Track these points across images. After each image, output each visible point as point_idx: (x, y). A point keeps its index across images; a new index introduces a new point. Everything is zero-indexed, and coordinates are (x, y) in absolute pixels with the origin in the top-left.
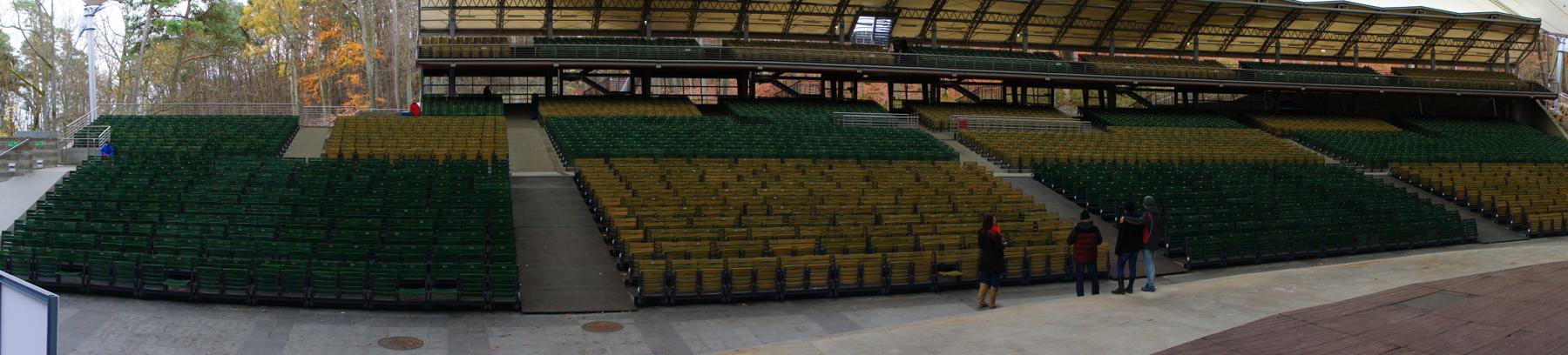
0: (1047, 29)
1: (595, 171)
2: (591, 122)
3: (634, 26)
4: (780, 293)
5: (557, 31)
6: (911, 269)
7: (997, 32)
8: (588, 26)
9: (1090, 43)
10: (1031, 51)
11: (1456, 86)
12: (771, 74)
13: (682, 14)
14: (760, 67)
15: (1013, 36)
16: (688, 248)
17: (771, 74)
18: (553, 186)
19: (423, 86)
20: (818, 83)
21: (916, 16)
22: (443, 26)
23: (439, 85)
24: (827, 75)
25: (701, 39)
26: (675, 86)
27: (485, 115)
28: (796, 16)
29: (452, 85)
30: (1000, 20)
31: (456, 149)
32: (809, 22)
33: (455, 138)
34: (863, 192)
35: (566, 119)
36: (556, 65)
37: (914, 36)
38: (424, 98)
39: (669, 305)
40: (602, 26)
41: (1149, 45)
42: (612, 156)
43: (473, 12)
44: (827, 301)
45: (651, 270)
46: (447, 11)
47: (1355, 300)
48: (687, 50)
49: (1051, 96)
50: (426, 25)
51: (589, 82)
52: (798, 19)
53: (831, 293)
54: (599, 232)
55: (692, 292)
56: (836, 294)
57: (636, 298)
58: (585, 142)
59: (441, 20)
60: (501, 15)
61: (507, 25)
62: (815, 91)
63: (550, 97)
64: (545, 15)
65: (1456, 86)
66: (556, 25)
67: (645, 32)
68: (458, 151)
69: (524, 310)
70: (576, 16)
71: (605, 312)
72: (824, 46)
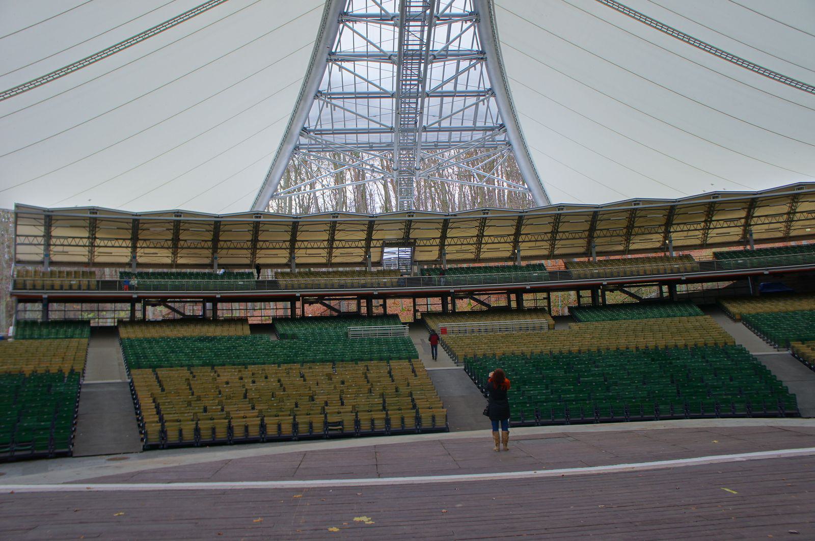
1: (144, 378)
2: (158, 342)
3: (508, 254)
7: (539, 248)
8: (169, 261)
9: (582, 250)
18: (113, 389)
19: (17, 312)
22: (39, 258)
23: (33, 312)
24: (360, 297)
26: (238, 310)
29: (46, 311)
32: (346, 253)
37: (435, 259)
38: (18, 323)
40: (180, 261)
41: (632, 247)
45: (153, 428)
47: (721, 428)
48: (534, 275)
49: (548, 298)
50: (21, 257)
54: (135, 415)
57: (144, 446)
58: (146, 357)
59: (37, 254)
61: (98, 259)
63: (133, 322)
64: (131, 252)
68: (43, 367)
70: (157, 254)
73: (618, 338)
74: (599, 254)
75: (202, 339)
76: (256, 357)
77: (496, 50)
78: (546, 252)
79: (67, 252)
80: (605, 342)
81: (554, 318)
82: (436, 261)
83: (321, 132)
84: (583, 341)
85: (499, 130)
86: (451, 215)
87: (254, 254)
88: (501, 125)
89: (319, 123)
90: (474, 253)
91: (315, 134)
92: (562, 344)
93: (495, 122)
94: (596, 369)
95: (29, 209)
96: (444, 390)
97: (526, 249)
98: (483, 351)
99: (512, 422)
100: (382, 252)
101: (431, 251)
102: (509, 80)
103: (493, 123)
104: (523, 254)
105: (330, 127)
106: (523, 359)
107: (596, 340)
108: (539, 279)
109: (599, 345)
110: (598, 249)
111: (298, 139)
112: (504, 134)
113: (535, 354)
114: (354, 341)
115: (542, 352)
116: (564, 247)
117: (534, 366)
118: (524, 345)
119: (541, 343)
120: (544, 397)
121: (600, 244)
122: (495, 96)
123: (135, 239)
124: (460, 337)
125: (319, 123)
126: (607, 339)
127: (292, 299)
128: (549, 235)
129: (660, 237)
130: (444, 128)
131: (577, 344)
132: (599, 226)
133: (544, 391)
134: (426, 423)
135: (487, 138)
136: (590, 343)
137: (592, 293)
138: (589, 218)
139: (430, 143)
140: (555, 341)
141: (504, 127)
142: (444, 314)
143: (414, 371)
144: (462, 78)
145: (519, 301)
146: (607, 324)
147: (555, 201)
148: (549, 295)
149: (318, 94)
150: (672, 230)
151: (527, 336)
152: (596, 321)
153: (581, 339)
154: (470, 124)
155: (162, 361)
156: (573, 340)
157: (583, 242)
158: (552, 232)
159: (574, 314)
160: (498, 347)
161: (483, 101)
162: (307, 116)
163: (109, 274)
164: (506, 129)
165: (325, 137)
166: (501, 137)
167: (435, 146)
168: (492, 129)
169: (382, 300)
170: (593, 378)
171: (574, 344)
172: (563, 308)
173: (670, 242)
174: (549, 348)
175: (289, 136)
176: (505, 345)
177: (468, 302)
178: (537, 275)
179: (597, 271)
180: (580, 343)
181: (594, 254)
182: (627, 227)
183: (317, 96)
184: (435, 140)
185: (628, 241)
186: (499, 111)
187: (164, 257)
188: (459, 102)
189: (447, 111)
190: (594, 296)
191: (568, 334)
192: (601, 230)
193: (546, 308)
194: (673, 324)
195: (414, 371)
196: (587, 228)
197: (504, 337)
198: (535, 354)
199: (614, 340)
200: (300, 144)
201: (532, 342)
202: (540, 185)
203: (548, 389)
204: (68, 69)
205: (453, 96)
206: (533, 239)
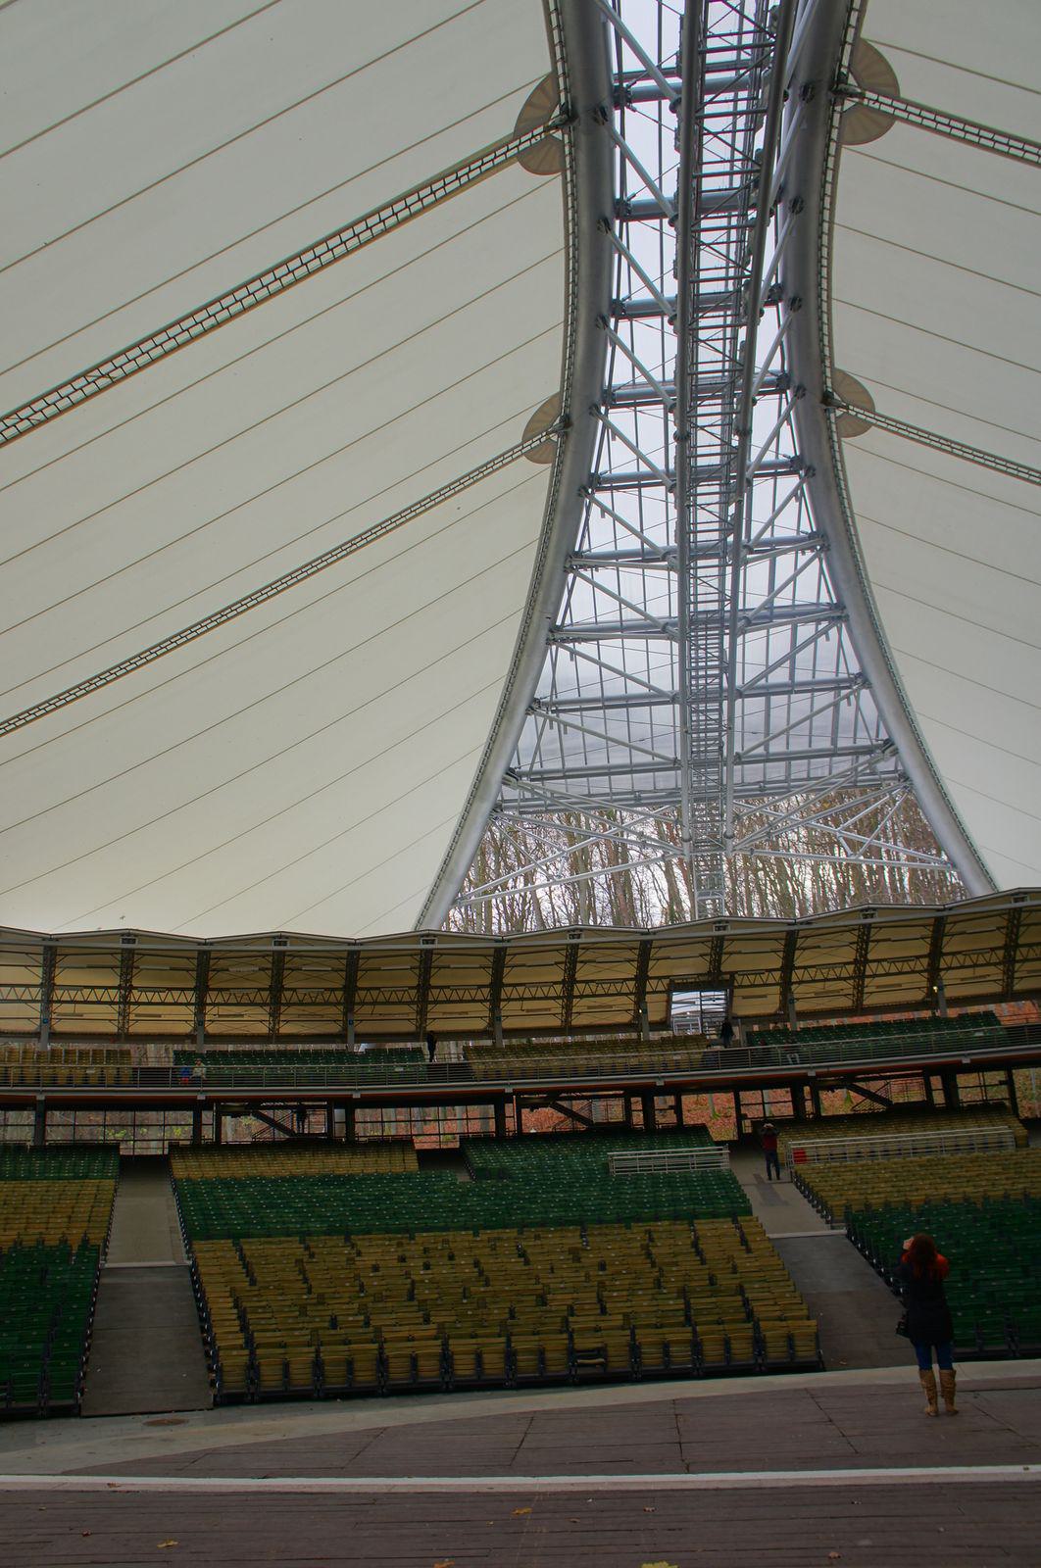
3: (920, 995)
4: (383, 1387)
8: (263, 1029)
11: (498, 1076)
13: (406, 1009)
16: (411, 1333)
18: (158, 1279)
27: (86, 1177)
31: (31, 1231)
33: (31, 1216)
35: (206, 1182)
39: (252, 1403)
40: (285, 1029)
42: (310, 1234)
43: (80, 1008)
44: (438, 1396)
46: (38, 1006)
48: (977, 1034)
49: (1009, 1083)
51: (561, 1109)
53: (758, 1369)
55: (307, 1385)
56: (256, 1398)
57: (215, 1396)
60: (124, 1015)
61: (137, 1028)
63: (197, 1147)
65: (498, 1076)
67: (937, 1002)
69: (84, 1413)
71: (176, 1411)
75: (326, 1180)
78: (996, 988)
82: (775, 1014)
83: (543, 776)
85: (883, 752)
91: (532, 780)
93: (873, 734)
98: (882, 1195)
100: (669, 1002)
101: (765, 996)
102: (896, 654)
104: (949, 993)
108: (985, 1043)
112: (894, 758)
115: (1006, 1196)
118: (968, 1181)
119: (1003, 1177)
123: (202, 989)
125: (537, 759)
130: (774, 754)
135: (860, 769)
140: (1034, 1172)
141: (892, 744)
143: (744, 1241)
144: (804, 657)
145: (950, 1089)
147: (1007, 882)
148: (1010, 1076)
151: (971, 1162)
154: (824, 743)
158: (1005, 947)
160: (914, 1187)
162: (515, 747)
163: (156, 1056)
166: (887, 765)
167: (761, 789)
176: (928, 1182)
177: (845, 1096)
178: (981, 1034)
183: (533, 709)
188: (801, 703)
189: (778, 720)
193: (1007, 1103)
206: (968, 962)
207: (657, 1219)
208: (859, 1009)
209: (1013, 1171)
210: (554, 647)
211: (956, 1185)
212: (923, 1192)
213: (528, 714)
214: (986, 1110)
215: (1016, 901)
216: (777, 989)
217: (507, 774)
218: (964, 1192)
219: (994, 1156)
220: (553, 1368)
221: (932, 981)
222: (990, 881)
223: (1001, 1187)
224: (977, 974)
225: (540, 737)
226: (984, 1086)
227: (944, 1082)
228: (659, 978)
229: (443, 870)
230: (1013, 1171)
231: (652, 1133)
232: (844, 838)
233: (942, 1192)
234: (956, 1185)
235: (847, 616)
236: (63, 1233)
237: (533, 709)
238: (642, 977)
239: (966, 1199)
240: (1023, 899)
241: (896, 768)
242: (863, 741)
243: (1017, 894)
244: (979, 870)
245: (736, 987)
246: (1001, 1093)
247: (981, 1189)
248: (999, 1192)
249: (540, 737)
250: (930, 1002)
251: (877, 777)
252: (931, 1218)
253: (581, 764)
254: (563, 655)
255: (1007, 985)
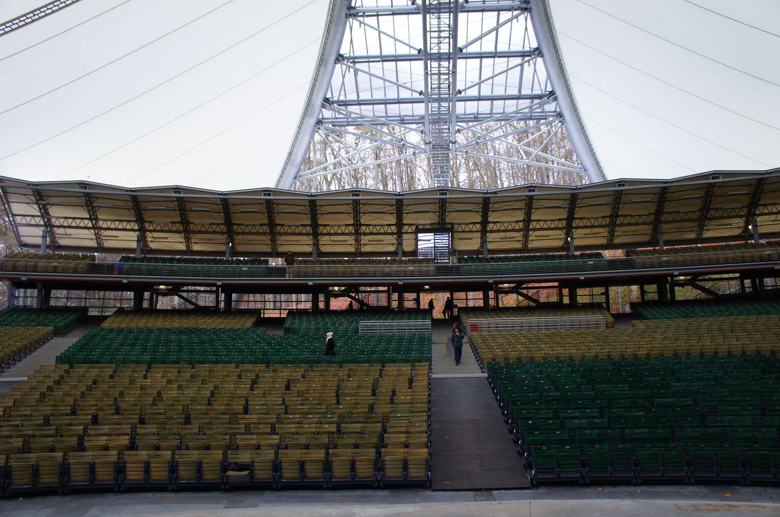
0: (595, 230)
3: (560, 243)
5: (490, 251)
6: (199, 466)
9: (646, 238)
10: (764, 241)
11: (306, 275)
12: (689, 277)
14: (676, 273)
15: (746, 228)
17: (689, 277)
20: (555, 291)
21: (549, 223)
25: (606, 251)
28: (616, 228)
30: (545, 226)
32: (376, 241)
34: (264, 393)
36: (491, 281)
40: (196, 247)
41: (706, 235)
43: (69, 231)
48: (590, 263)
49: (607, 294)
52: (365, 239)
62: (554, 299)
65: (306, 275)
66: (490, 246)
72: (737, 247)
73: (699, 339)
74: (667, 243)
75: (190, 331)
76: (512, 349)
77: (545, 9)
78: (604, 241)
79: (70, 235)
80: (683, 344)
81: (613, 315)
82: (478, 250)
83: (346, 104)
84: (653, 342)
85: (548, 98)
86: (491, 193)
87: (274, 241)
88: (551, 92)
89: (343, 93)
90: (521, 242)
91: (339, 105)
92: (624, 346)
93: (543, 88)
94: (678, 384)
95: (17, 183)
96: (448, 409)
97: (581, 238)
98: (517, 353)
99: (541, 476)
100: (417, 240)
101: (471, 239)
102: (558, 34)
103: (541, 90)
104: (577, 243)
105: (354, 97)
106: (569, 366)
107: (670, 342)
108: (594, 268)
109: (675, 348)
110: (666, 237)
111: (321, 111)
112: (554, 103)
113: (587, 358)
114: (360, 338)
115: (596, 357)
116: (625, 233)
117: (584, 376)
118: (573, 346)
119: (596, 344)
120: (596, 431)
121: (668, 231)
122: (542, 56)
123: (140, 220)
124: (494, 335)
125: (343, 93)
126: (686, 341)
127: (315, 290)
128: (608, 220)
129: (740, 222)
130: (483, 97)
131: (645, 346)
132: (669, 207)
133: (597, 421)
134: (393, 472)
135: (534, 107)
136: (662, 345)
137: (658, 287)
138: (655, 198)
139: (468, 114)
140: (615, 342)
141: (554, 94)
142: (485, 310)
143: (411, 381)
144: (504, 31)
145: (573, 296)
146: (682, 323)
147: (612, 175)
148: (607, 291)
149: (340, 58)
150: (757, 212)
151: (578, 335)
152: (667, 318)
153: (649, 339)
154: (514, 92)
155: (493, 348)
156: (639, 341)
157: (648, 229)
158: (611, 216)
159: (638, 310)
160: (538, 349)
161: (528, 61)
162: (329, 84)
163: (113, 259)
164: (556, 97)
165: (351, 108)
166: (550, 107)
167: (475, 118)
168: (540, 97)
169: (416, 294)
170: (463, 169)
171: (640, 346)
172: (623, 305)
173: (755, 226)
174: (606, 350)
175: (310, 107)
176: (548, 346)
177: (516, 298)
178: (592, 263)
179: (667, 259)
180: (649, 346)
181: (661, 243)
182: (701, 210)
183: (338, 60)
184: (475, 111)
185: (701, 228)
186: (549, 76)
187: (175, 242)
188: (501, 64)
189: (487, 73)
190: (661, 291)
191: (632, 333)
192: (670, 213)
193: (604, 305)
194: (710, 335)
195: (411, 381)
196: (653, 211)
197: (548, 336)
198: (587, 358)
199: (696, 341)
200: (323, 118)
201: (584, 343)
202: (597, 163)
203: (603, 417)
204: (35, 15)
205: (494, 57)
206: (589, 224)
207: (217, 363)
208: (525, 249)
209: (602, 341)
210: (351, 19)
211: (565, 348)
212: (543, 352)
213: (335, 63)
214: (592, 307)
215: (619, 186)
216: (479, 235)
217: (324, 101)
218: (570, 353)
219: (592, 332)
220: (208, 477)
221: (567, 235)
222: (603, 176)
223: (593, 351)
224: (593, 232)
225: (344, 77)
226: (592, 295)
227: (570, 292)
228: (410, 225)
229: (288, 159)
230: (602, 341)
231: (402, 312)
232: (523, 150)
233: (555, 352)
234: (565, 348)
235: (531, 8)
236: (701, 349)
237: (338, 60)
238: (400, 224)
239: (571, 358)
240: (623, 185)
241: (556, 109)
242: (537, 92)
243: (620, 182)
244: (599, 173)
245: (455, 232)
246: (602, 299)
247: (581, 352)
248: (592, 353)
249: (344, 77)
250: (566, 247)
251: (544, 114)
252: (544, 369)
253: (369, 97)
254: (355, 23)
255: (610, 240)
